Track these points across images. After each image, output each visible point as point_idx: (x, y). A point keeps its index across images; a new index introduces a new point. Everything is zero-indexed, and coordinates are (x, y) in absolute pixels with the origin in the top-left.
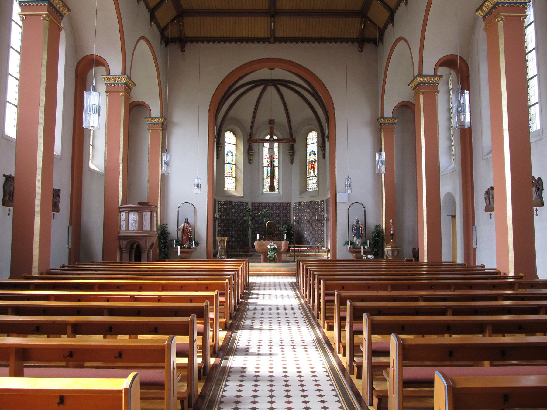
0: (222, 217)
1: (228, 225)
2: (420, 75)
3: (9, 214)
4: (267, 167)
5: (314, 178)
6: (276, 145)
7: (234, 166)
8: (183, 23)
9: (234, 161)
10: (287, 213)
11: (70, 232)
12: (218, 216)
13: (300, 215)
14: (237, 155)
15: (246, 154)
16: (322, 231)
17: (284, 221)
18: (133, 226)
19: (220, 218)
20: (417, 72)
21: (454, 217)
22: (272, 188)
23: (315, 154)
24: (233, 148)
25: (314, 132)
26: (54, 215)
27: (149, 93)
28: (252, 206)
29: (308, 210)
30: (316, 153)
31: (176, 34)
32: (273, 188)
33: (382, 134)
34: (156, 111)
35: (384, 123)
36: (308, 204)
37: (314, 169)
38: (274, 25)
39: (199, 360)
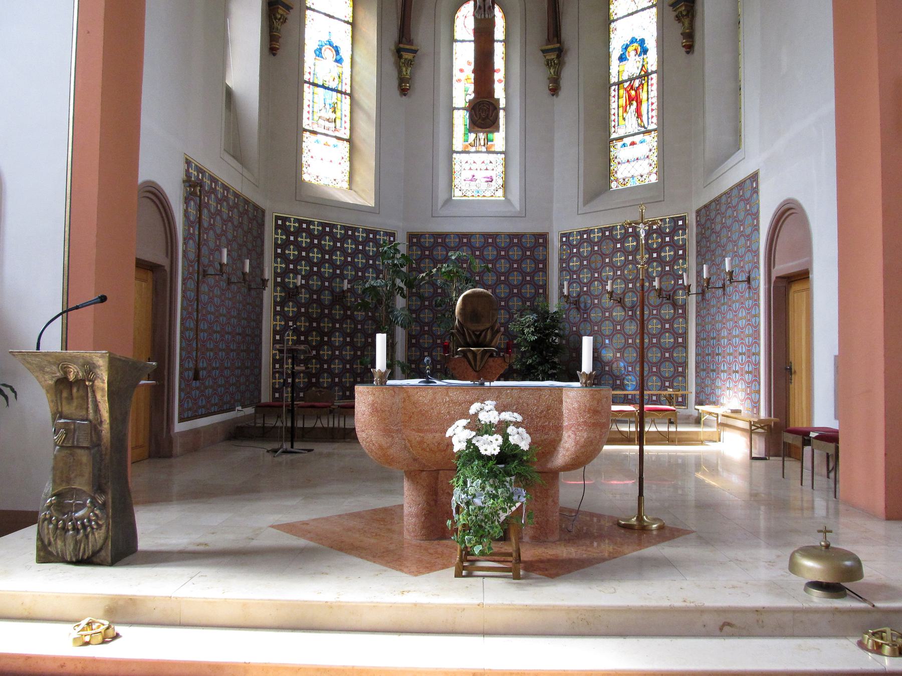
1: (314, 310)
10: (537, 270)
13: (585, 276)
14: (357, 58)
15: (390, 58)
16: (676, 335)
17: (524, 300)
24: (342, 36)
28: (411, 245)
29: (619, 259)
30: (651, 45)
36: (618, 233)
37: (639, 103)
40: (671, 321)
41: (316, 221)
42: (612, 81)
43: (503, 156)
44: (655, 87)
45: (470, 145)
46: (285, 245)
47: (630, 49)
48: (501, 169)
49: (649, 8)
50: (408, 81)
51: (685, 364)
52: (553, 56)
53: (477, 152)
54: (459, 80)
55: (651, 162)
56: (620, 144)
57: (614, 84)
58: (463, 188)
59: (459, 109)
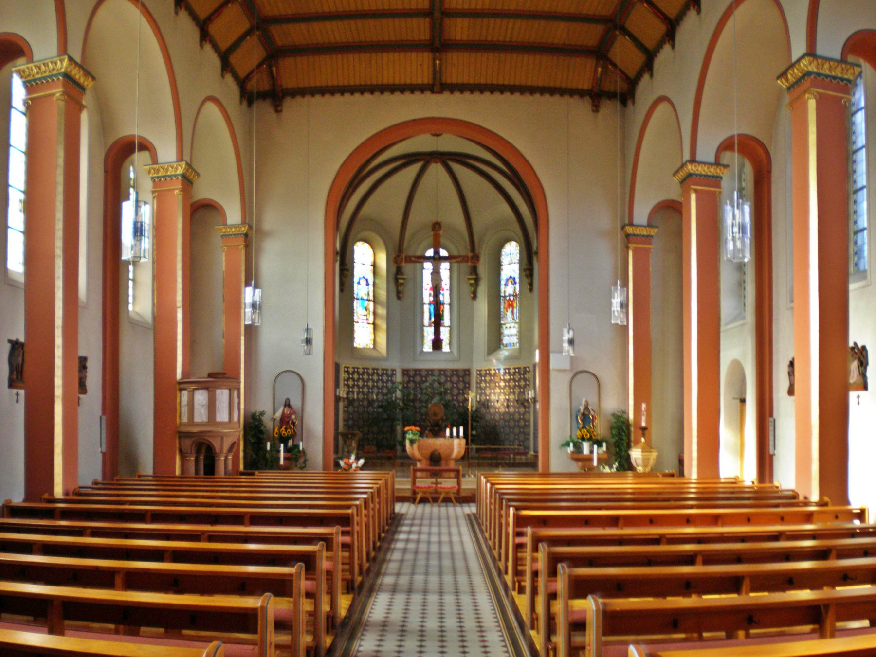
0: (351, 396)
2: (693, 160)
3: (17, 401)
4: (430, 304)
6: (445, 267)
7: (371, 304)
8: (277, 68)
9: (371, 294)
11: (104, 426)
12: (342, 393)
18: (201, 415)
19: (348, 398)
20: (687, 156)
21: (743, 401)
22: (437, 344)
23: (515, 283)
25: (514, 243)
26: (79, 398)
27: (223, 190)
28: (404, 375)
30: (517, 280)
31: (266, 86)
32: (437, 345)
33: (631, 253)
34: (234, 215)
35: (634, 235)
37: (513, 308)
38: (440, 65)
39: (326, 608)
46: (348, 380)
51: (529, 434)
52: (473, 281)
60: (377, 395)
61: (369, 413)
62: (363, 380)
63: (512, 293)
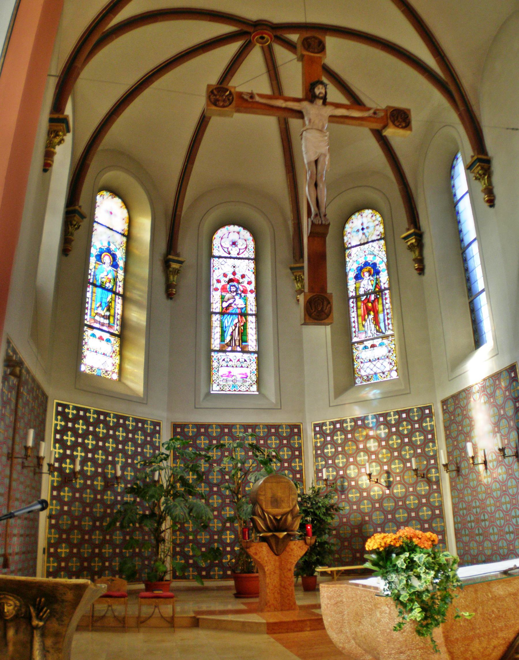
5: (377, 342)
30: (382, 267)
40: (427, 496)
41: (92, 409)
42: (351, 294)
43: (256, 355)
44: (388, 301)
45: (227, 344)
46: (63, 431)
47: (365, 270)
48: (254, 366)
49: (378, 240)
50: (174, 286)
53: (232, 351)
54: (216, 289)
55: (391, 361)
56: (361, 347)
57: (352, 297)
58: (221, 383)
59: (216, 313)
60: (123, 468)
61: (105, 506)
62: (95, 435)
63: (371, 288)
